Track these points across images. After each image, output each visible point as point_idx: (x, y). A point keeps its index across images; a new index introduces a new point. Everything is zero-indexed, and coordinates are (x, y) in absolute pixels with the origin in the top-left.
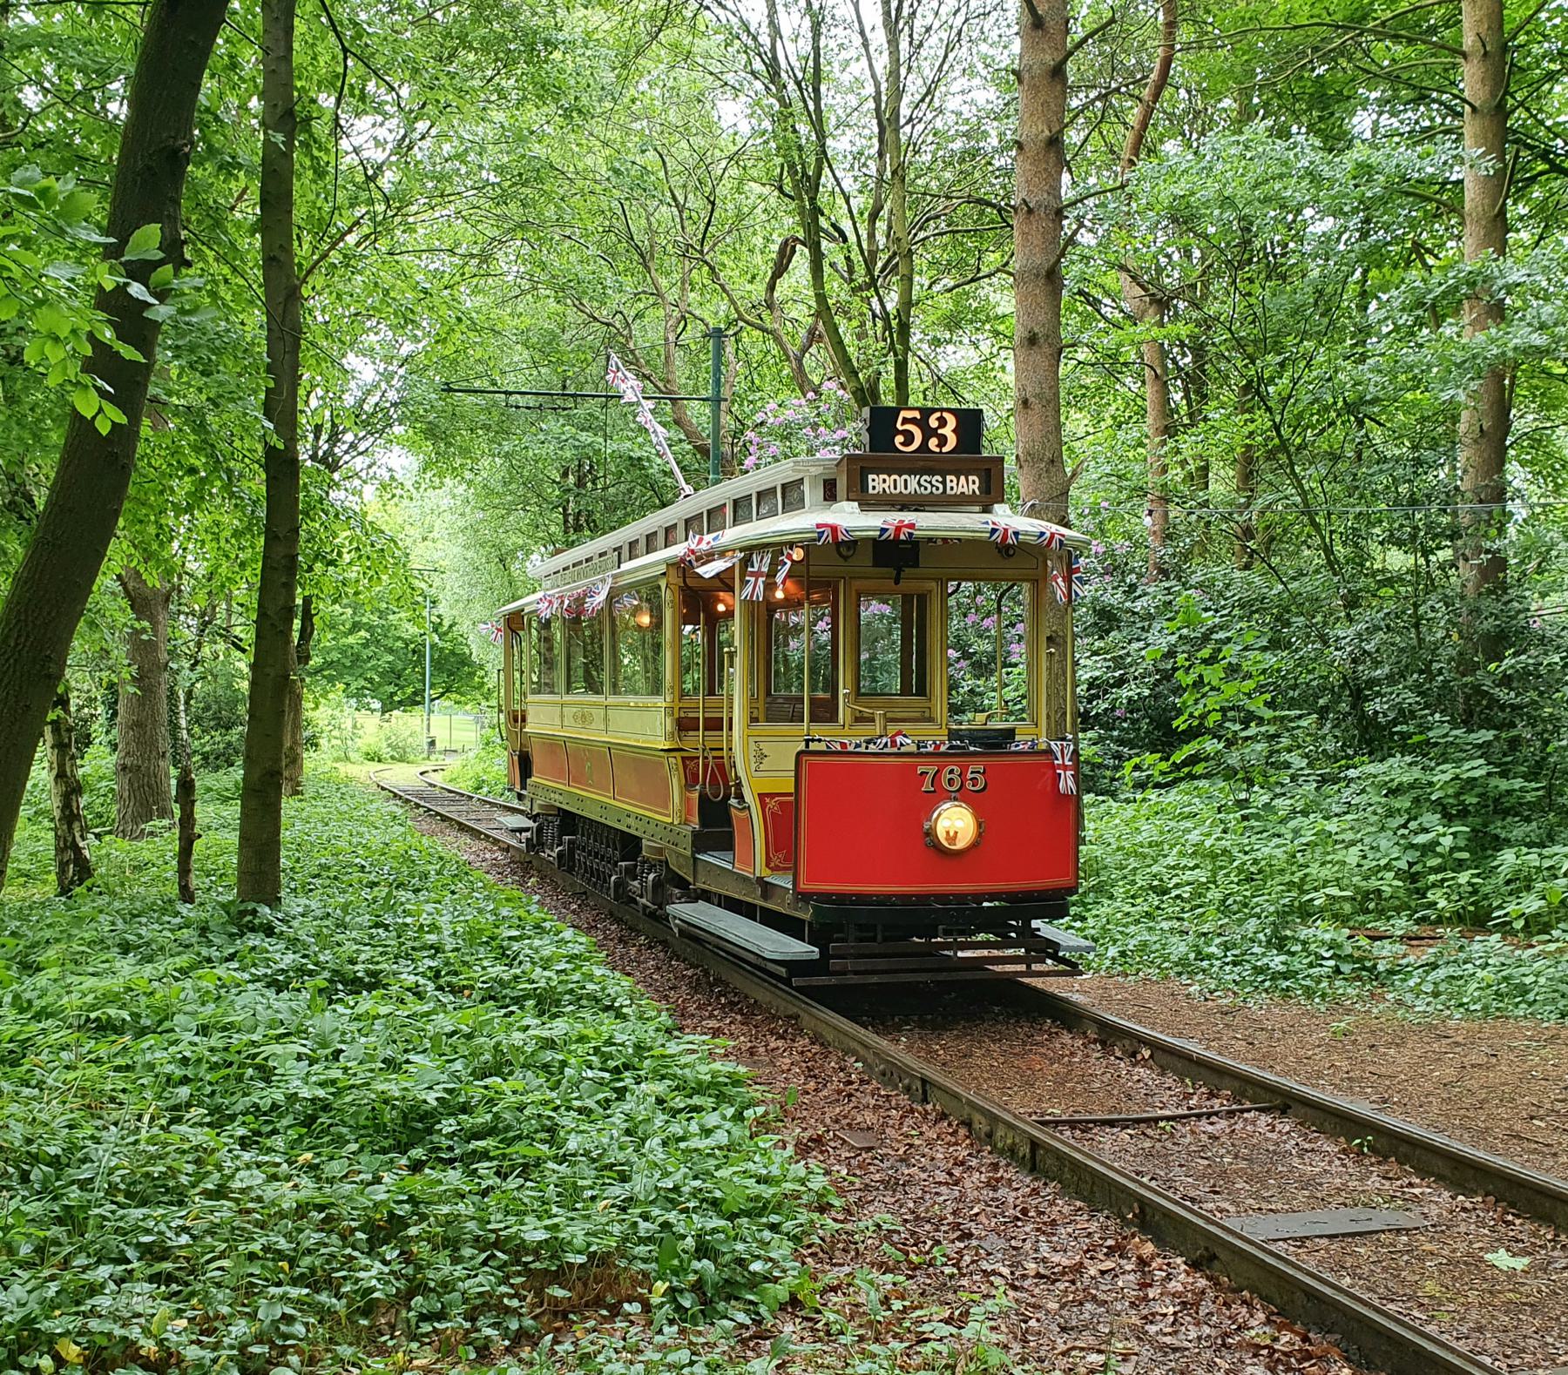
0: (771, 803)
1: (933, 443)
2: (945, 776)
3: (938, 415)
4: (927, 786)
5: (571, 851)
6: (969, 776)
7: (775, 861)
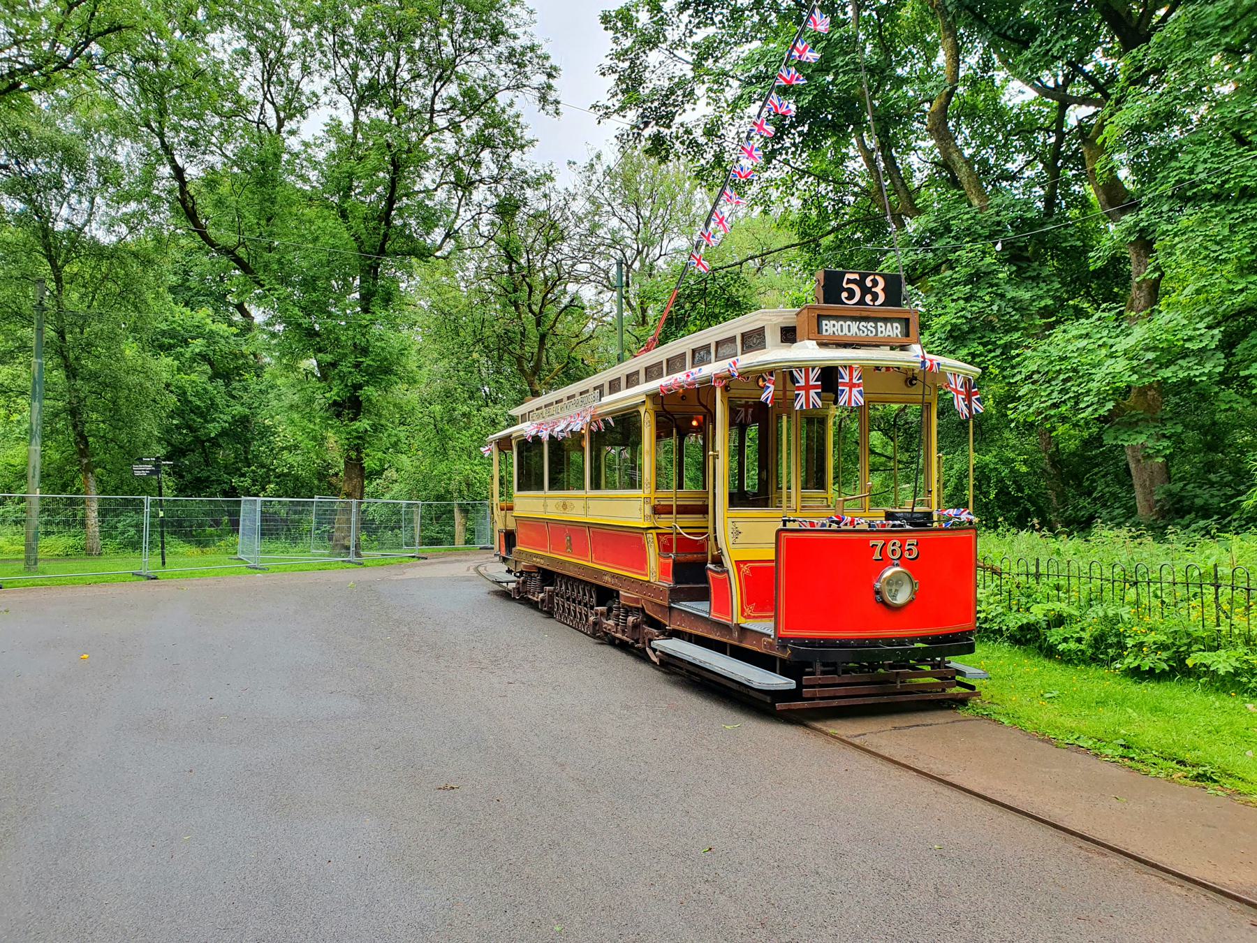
0: (744, 568)
2: (890, 548)
4: (877, 556)
5: (551, 597)
7: (748, 612)
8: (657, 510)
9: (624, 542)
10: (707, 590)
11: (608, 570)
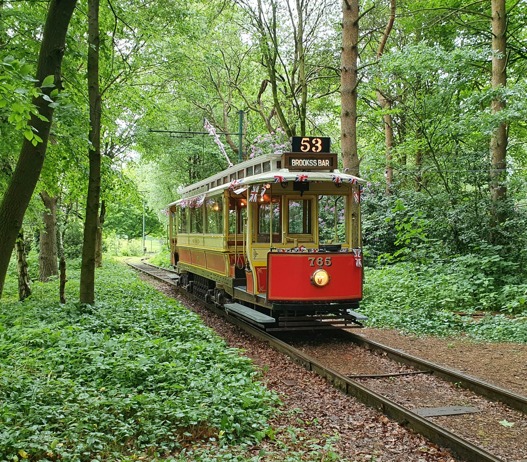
0: (259, 270)
1: (314, 149)
2: (318, 261)
3: (315, 139)
4: (312, 264)
5: (192, 286)
6: (326, 261)
7: (261, 289)
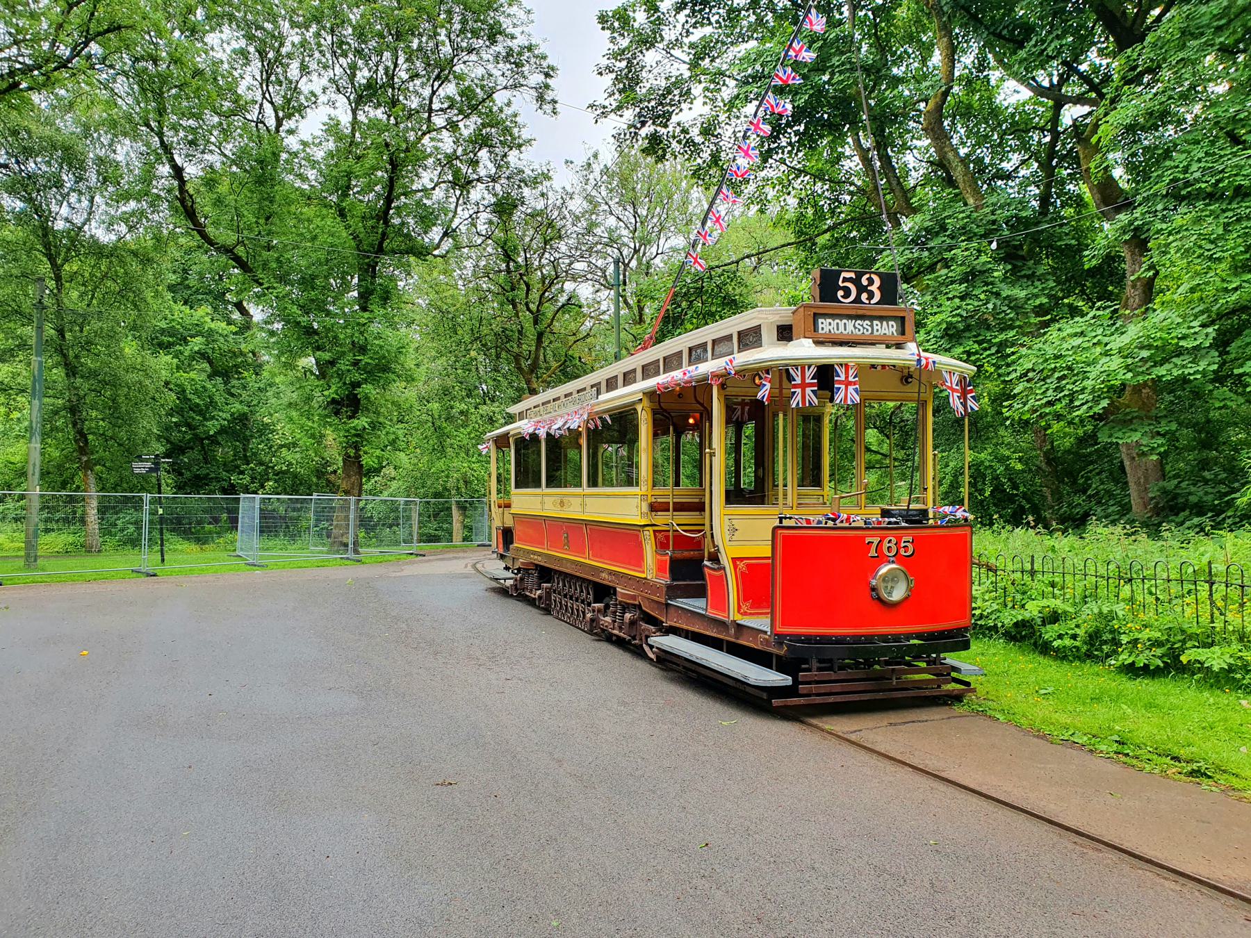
0: (741, 565)
2: (886, 545)
4: (873, 553)
5: (548, 594)
7: (744, 608)
8: (654, 508)
9: (621, 539)
10: (704, 587)
11: (605, 567)
